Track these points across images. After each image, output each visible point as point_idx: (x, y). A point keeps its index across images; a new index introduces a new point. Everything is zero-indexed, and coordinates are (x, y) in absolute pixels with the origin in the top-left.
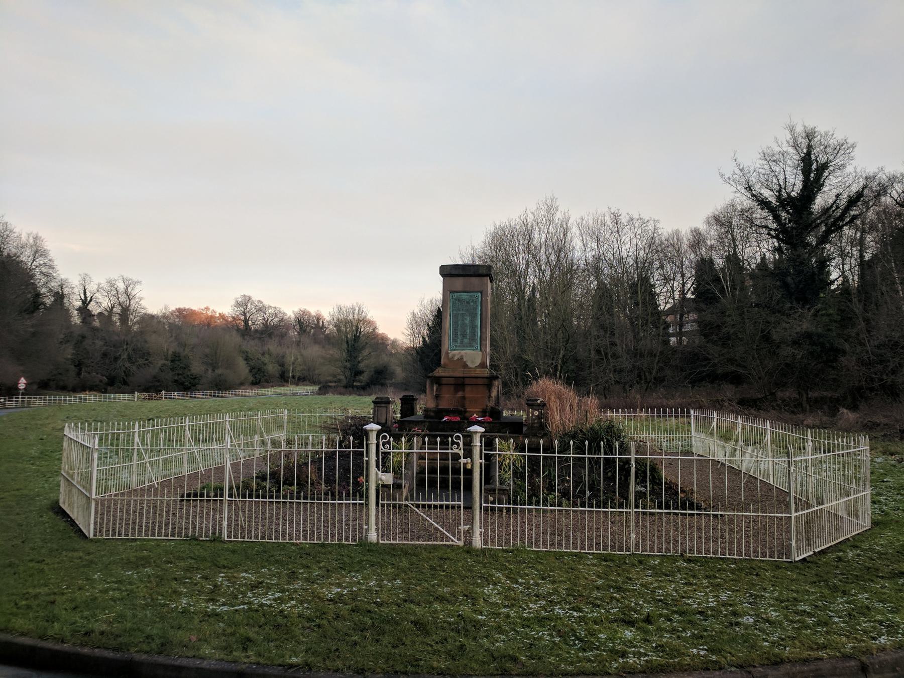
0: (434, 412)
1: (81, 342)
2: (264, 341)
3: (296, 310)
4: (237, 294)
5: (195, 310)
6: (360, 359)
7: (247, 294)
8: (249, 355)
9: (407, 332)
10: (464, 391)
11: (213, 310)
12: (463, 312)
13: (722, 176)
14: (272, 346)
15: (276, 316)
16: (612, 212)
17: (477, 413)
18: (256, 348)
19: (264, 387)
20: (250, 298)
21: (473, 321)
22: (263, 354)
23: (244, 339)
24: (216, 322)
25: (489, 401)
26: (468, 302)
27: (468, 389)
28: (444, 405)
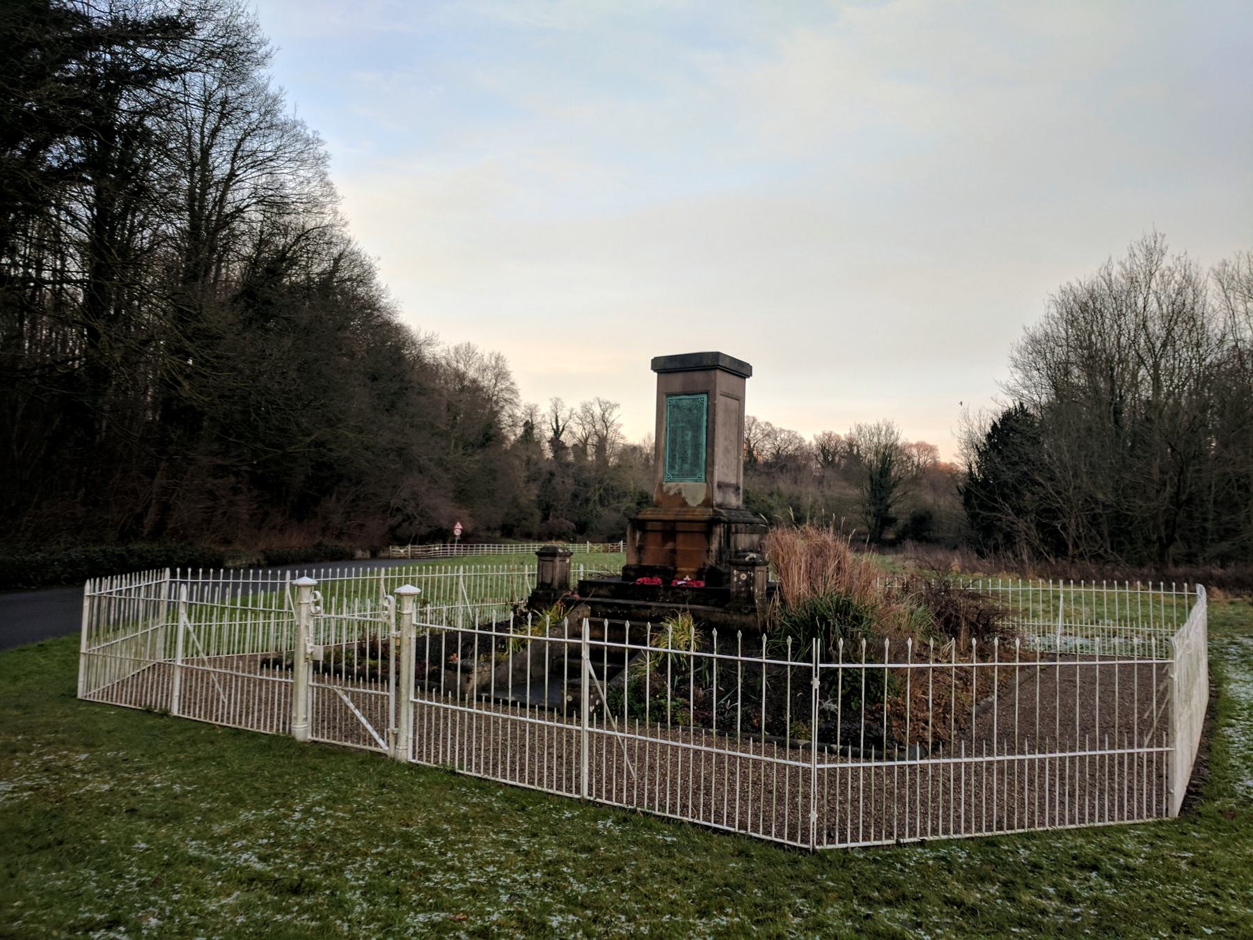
1: (550, 481)
2: (773, 477)
3: (819, 433)
6: (889, 501)
8: (750, 495)
10: (675, 541)
14: (784, 484)
17: (690, 573)
18: (762, 486)
21: (696, 438)
22: (771, 495)
26: (690, 410)
27: (680, 538)
28: (648, 561)
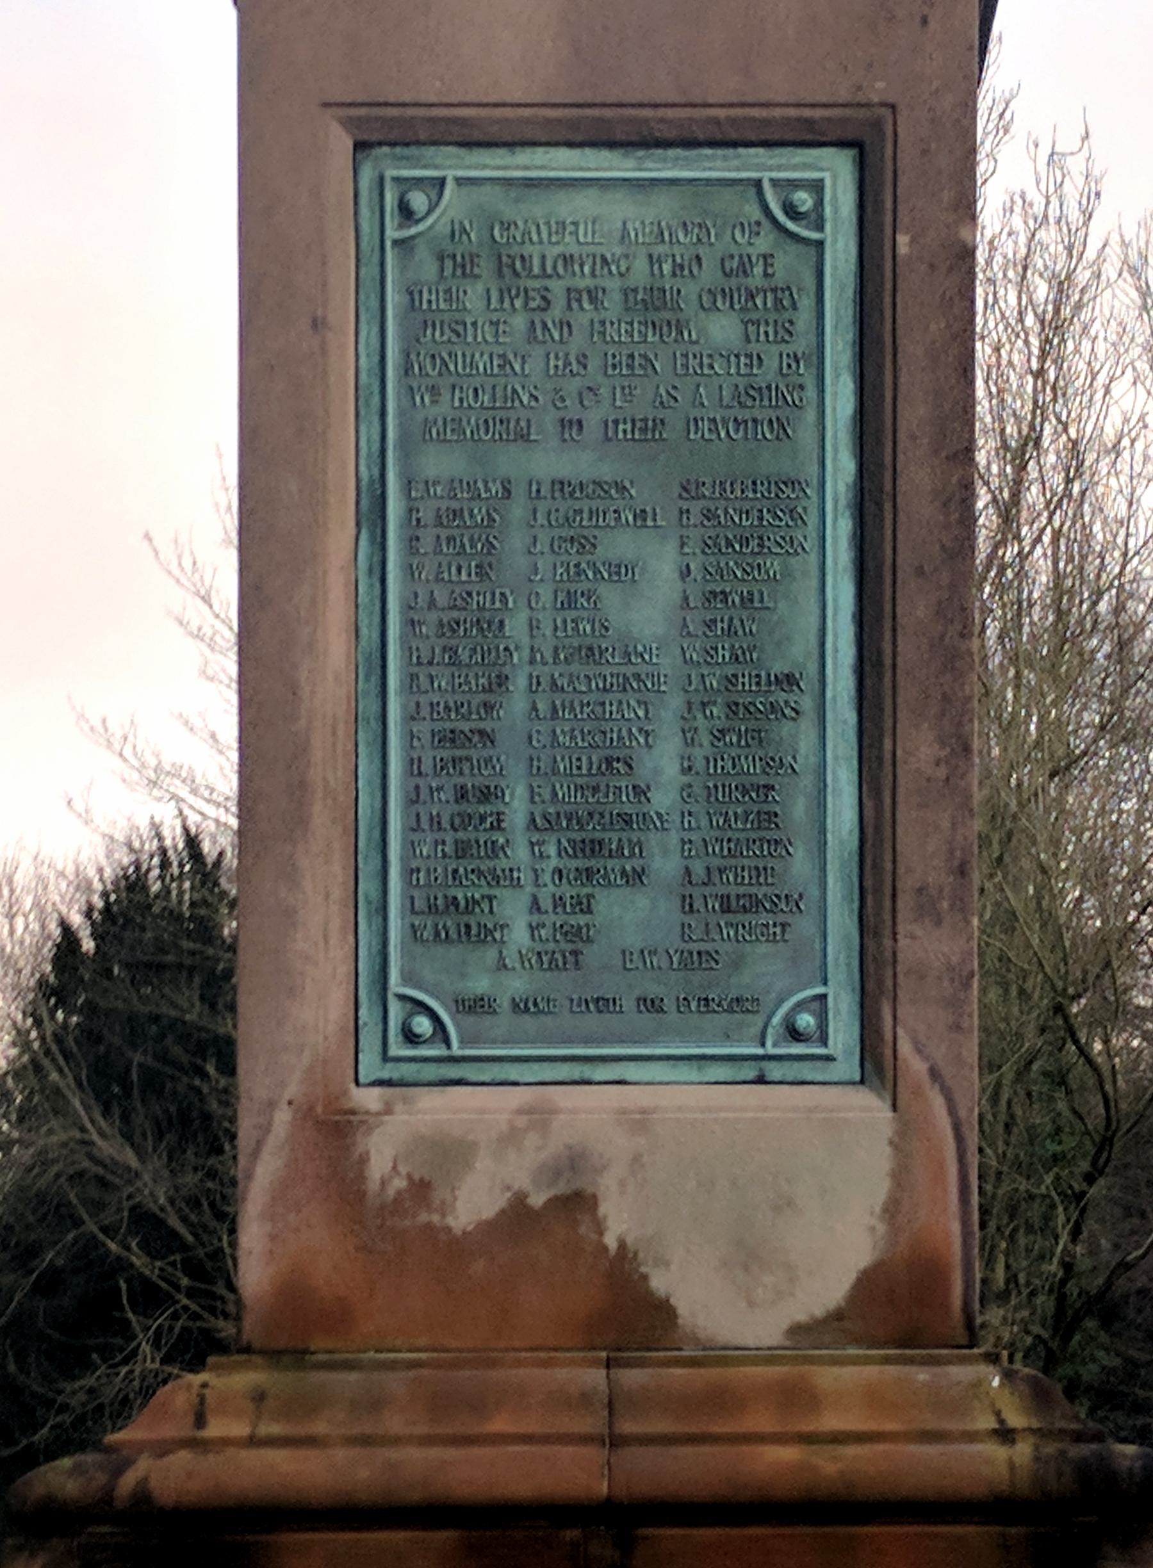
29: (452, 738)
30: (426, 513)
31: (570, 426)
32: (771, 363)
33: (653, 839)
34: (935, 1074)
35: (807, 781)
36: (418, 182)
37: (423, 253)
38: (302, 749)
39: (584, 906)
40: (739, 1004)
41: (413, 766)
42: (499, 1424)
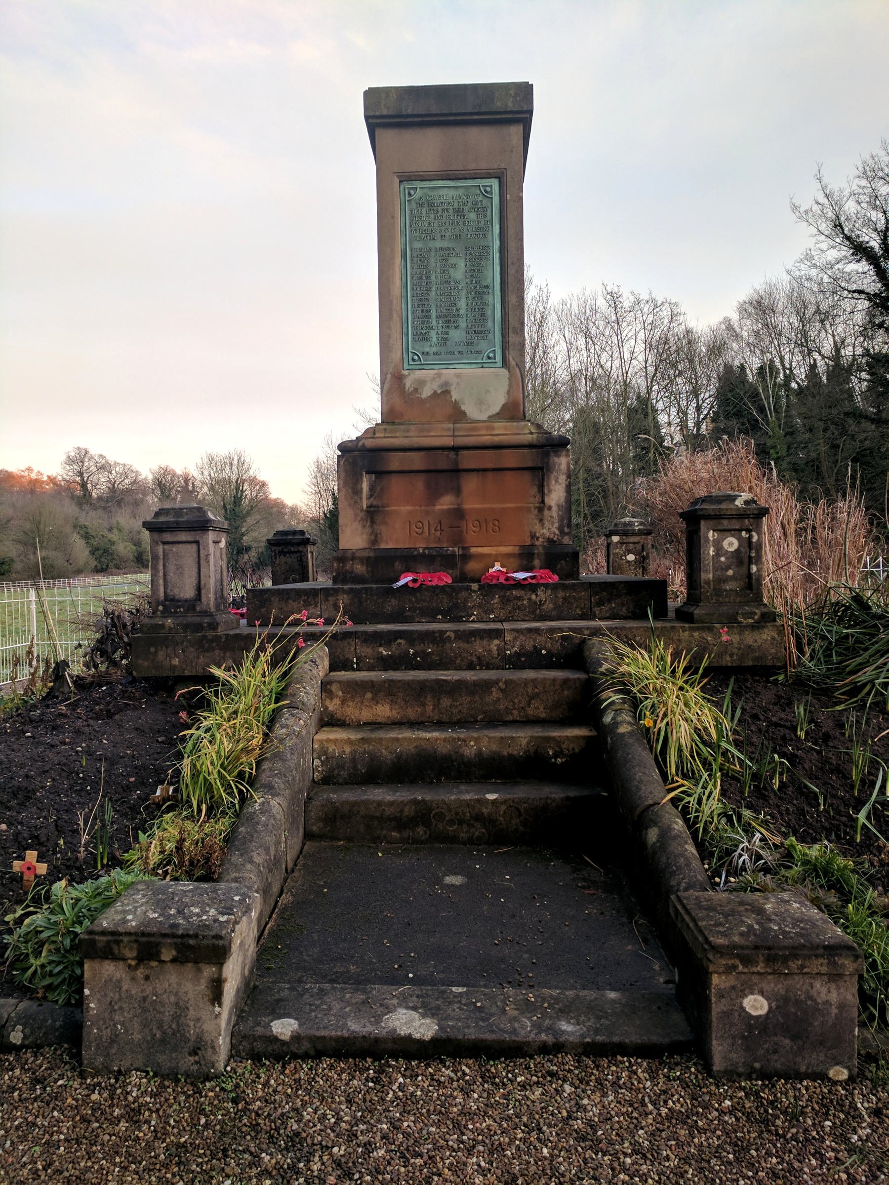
0: (367, 561)
2: (111, 512)
3: (155, 468)
4: (68, 446)
5: (11, 473)
7: (82, 446)
8: (89, 530)
9: (310, 490)
10: (458, 491)
11: (39, 472)
12: (445, 244)
13: (795, 208)
15: (127, 477)
16: (609, 291)
17: (503, 558)
18: (100, 521)
19: (112, 575)
20: (86, 452)
21: (475, 271)
22: (110, 530)
23: (81, 508)
24: (43, 488)
25: (541, 520)
26: (459, 212)
27: (470, 484)
29: (421, 300)
30: (415, 255)
31: (443, 237)
32: (482, 223)
33: (460, 320)
34: (517, 365)
35: (491, 307)
36: (412, 188)
37: (413, 202)
38: (391, 302)
39: (447, 333)
40: (478, 352)
41: (413, 306)
42: (432, 434)
